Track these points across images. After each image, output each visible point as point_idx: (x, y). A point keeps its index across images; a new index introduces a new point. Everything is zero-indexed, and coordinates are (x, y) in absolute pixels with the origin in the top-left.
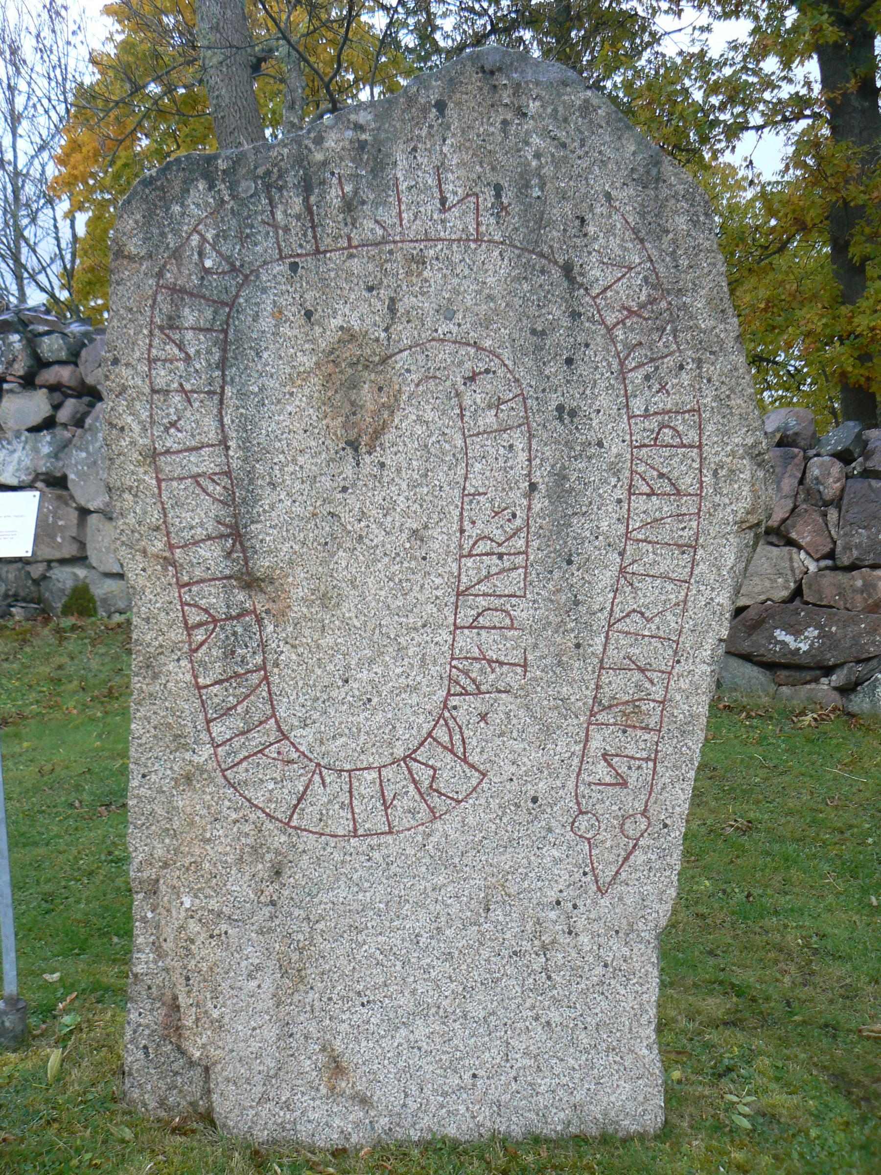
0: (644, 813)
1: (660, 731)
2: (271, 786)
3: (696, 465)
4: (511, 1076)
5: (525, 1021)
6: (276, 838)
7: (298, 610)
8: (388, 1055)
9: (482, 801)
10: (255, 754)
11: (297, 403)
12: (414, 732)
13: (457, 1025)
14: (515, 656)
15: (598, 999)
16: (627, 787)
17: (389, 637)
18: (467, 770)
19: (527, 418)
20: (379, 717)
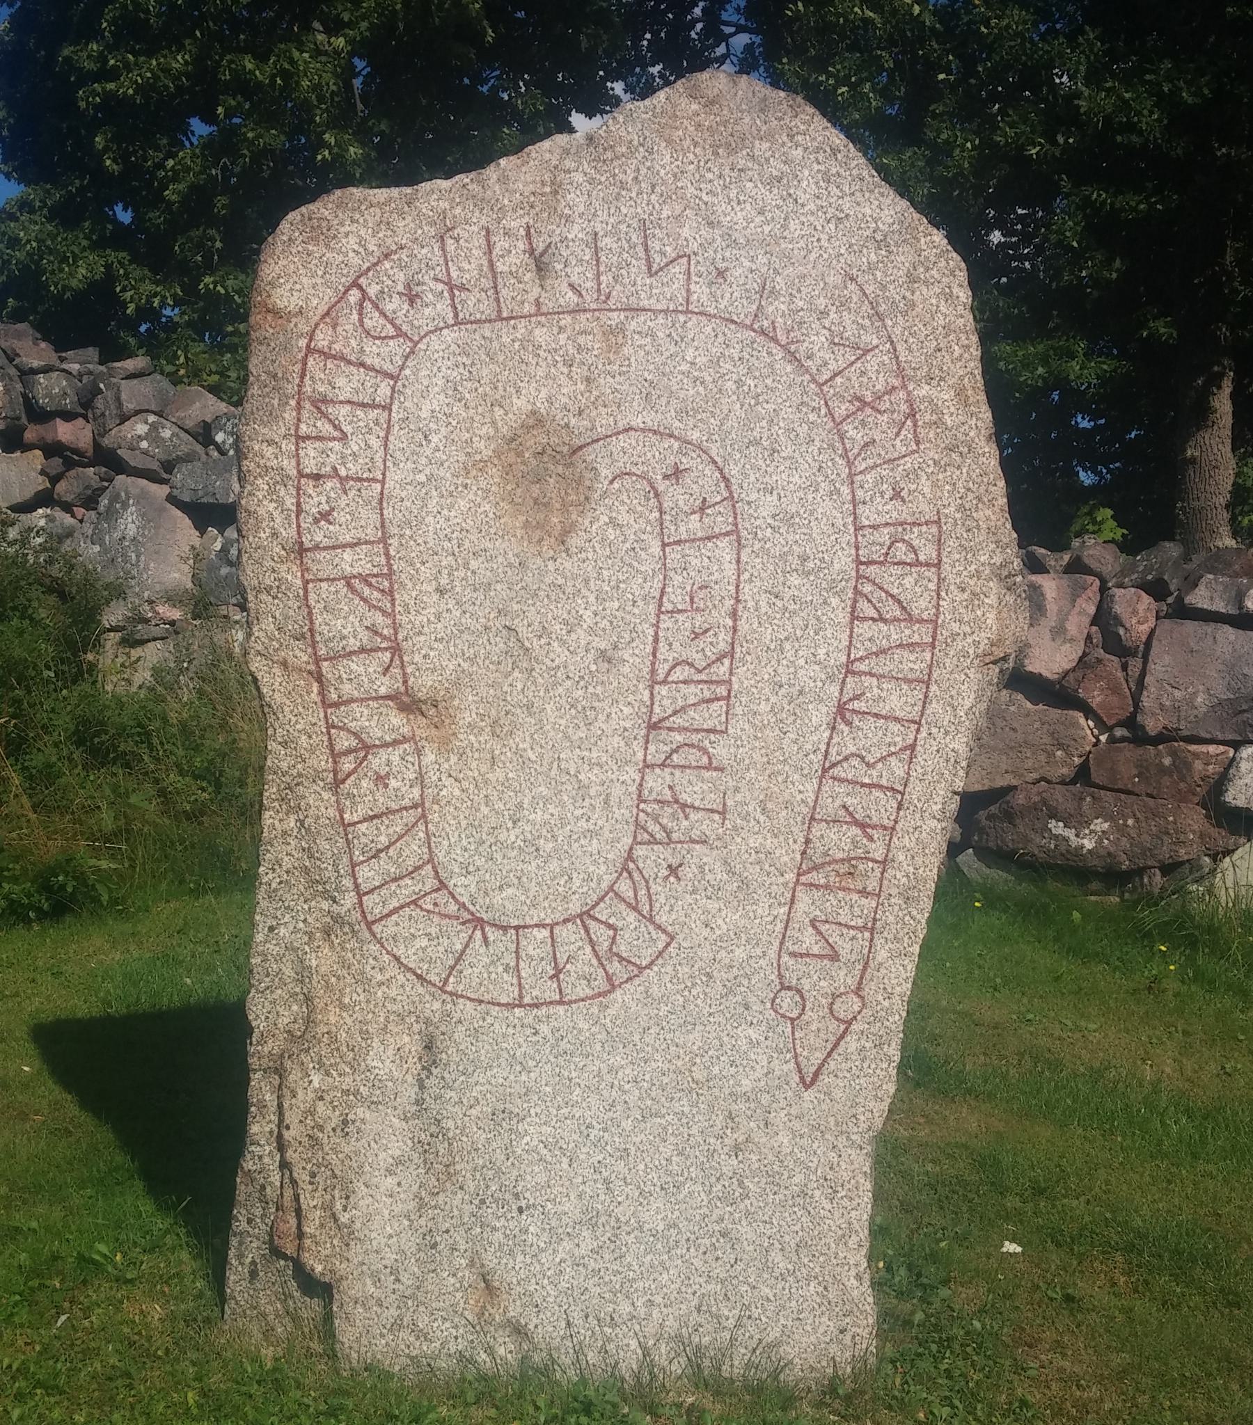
0: (858, 991)
1: (879, 896)
2: (425, 942)
3: (932, 586)
4: (693, 1304)
5: (711, 1236)
6: (427, 1005)
7: (465, 739)
8: (549, 1273)
9: (669, 969)
10: (408, 904)
11: (471, 496)
12: (593, 885)
13: (631, 1239)
14: (713, 801)
15: (799, 1214)
16: (838, 960)
17: (568, 773)
18: (653, 933)
19: (736, 525)
20: (554, 866)
